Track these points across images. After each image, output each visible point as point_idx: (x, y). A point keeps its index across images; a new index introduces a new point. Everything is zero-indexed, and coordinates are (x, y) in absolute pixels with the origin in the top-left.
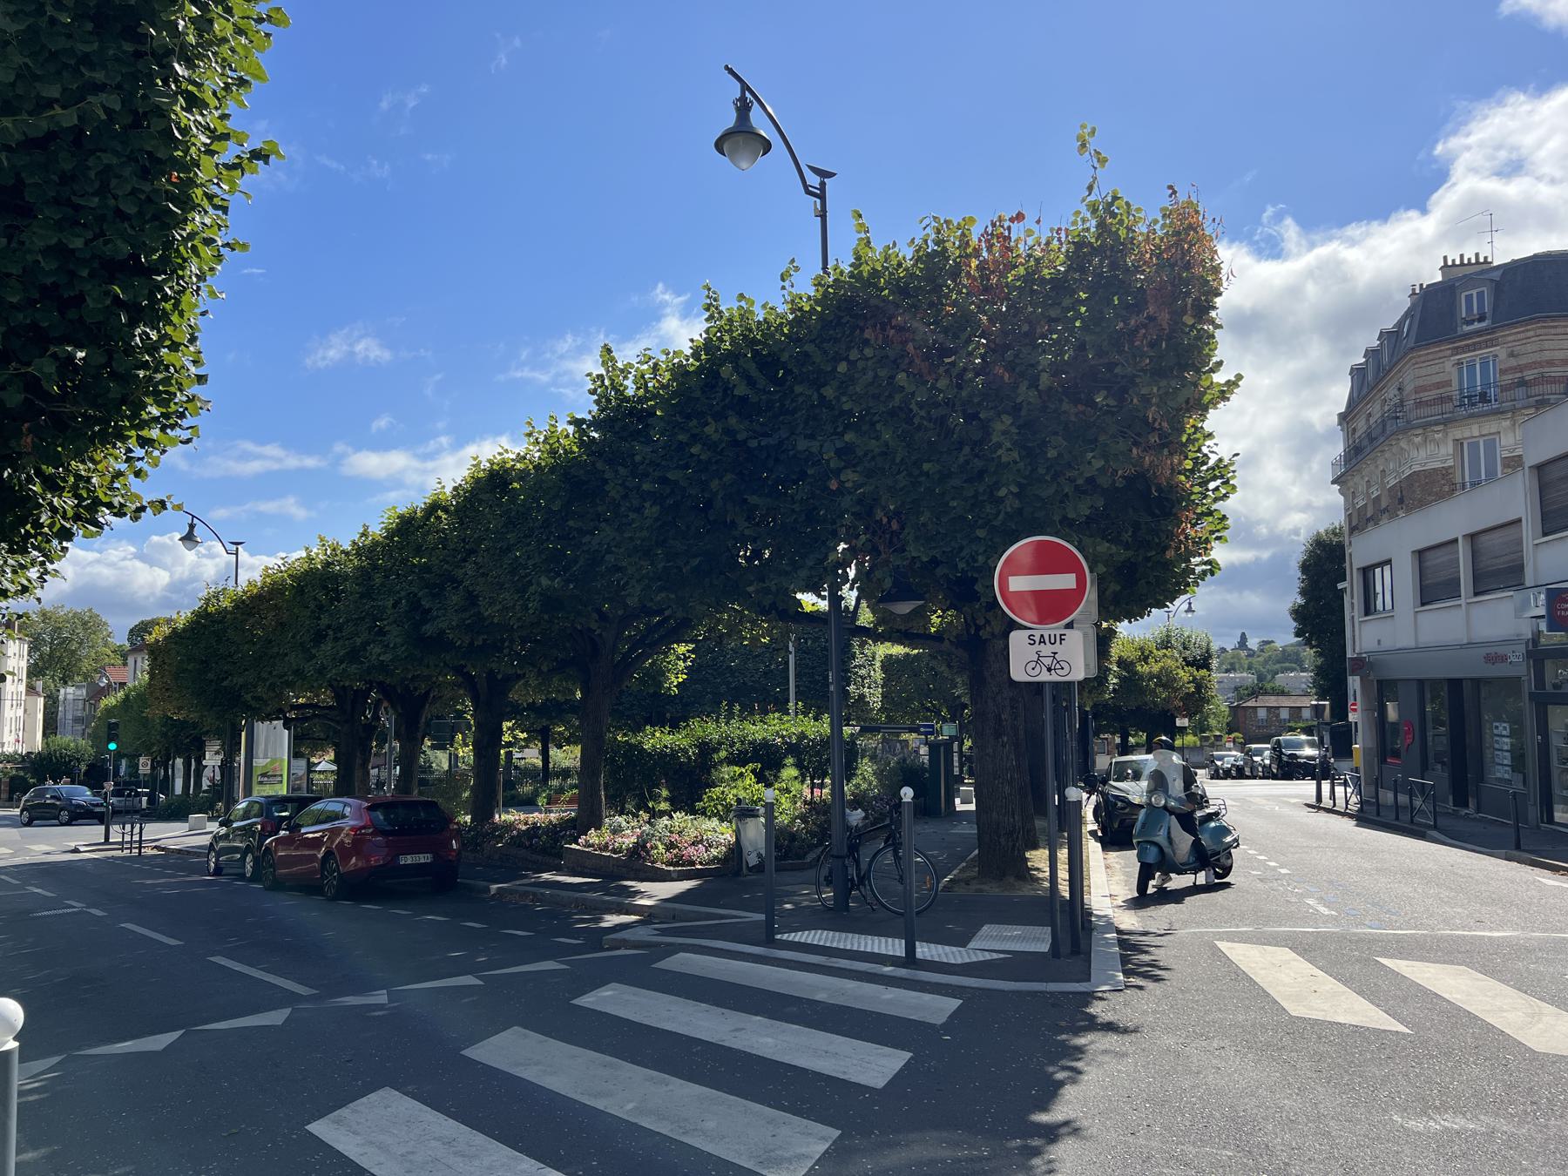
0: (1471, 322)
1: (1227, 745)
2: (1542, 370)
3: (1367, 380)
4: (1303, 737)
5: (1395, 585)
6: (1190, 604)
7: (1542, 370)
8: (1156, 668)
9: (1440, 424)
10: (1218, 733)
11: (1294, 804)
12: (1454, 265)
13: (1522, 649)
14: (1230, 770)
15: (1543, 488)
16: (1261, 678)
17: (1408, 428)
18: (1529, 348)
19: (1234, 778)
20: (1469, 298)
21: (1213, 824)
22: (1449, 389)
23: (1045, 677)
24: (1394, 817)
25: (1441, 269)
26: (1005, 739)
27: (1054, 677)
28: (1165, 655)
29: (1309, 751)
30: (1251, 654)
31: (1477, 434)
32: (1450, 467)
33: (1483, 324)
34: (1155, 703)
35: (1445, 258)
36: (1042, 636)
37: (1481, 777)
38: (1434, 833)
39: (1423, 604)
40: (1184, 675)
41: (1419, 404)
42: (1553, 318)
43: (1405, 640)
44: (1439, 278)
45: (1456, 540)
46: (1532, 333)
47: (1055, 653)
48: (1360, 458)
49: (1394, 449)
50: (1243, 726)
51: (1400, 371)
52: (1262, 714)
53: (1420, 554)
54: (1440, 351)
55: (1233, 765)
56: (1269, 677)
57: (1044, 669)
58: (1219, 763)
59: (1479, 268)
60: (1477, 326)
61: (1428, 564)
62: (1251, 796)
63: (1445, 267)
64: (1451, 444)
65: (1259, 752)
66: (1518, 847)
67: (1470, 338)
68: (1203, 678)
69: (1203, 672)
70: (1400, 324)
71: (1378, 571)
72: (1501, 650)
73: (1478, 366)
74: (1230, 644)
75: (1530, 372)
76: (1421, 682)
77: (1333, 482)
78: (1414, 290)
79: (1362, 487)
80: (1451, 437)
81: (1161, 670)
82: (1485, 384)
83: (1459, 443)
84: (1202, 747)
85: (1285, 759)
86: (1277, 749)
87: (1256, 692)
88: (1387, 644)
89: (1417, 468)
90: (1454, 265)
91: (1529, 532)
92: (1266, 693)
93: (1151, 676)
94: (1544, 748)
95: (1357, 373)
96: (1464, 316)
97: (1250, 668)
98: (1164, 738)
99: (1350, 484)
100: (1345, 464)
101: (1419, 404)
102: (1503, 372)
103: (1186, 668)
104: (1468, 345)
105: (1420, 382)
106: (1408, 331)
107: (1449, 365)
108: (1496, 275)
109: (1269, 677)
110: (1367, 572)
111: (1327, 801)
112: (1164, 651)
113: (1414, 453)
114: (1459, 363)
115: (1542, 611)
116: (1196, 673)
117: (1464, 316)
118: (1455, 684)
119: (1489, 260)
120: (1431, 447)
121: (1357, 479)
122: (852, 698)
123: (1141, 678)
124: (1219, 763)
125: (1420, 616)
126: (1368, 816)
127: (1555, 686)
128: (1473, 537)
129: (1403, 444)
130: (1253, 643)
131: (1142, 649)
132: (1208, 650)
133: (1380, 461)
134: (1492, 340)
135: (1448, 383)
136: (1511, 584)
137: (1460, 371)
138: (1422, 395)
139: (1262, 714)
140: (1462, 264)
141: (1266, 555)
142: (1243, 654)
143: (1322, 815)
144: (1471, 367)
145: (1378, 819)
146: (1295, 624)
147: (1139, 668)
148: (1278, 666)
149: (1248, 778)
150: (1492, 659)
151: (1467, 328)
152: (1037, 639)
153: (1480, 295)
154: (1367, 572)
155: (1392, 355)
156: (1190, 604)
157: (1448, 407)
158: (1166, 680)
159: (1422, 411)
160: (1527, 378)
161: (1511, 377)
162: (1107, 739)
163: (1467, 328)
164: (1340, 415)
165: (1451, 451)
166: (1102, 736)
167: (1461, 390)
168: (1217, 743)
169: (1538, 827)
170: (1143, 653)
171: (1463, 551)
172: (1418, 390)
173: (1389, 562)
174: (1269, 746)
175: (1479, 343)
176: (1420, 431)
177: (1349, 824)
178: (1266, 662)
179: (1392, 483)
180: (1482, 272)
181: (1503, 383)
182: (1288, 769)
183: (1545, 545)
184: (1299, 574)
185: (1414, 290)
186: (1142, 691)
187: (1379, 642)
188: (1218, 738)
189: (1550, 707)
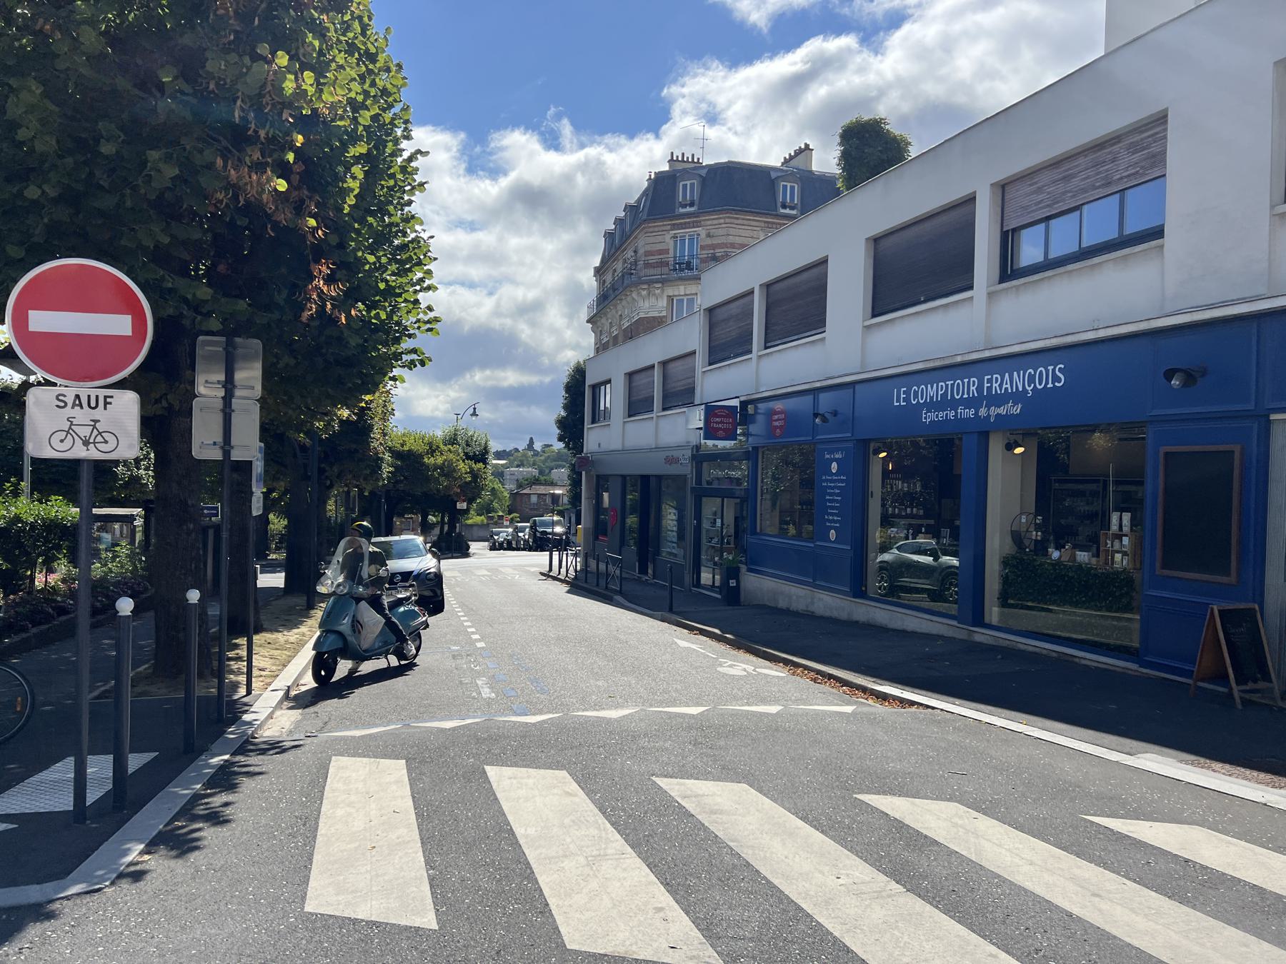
0: (685, 206)
1: (505, 523)
2: (726, 250)
3: (616, 242)
4: (556, 518)
5: (612, 399)
6: (475, 409)
7: (726, 250)
8: (440, 460)
9: (660, 282)
10: (501, 514)
11: (533, 572)
12: (677, 160)
13: (688, 453)
14: (503, 542)
15: (712, 326)
16: (541, 472)
17: (637, 284)
18: (721, 232)
19: (505, 549)
20: (685, 186)
21: (402, 609)
22: (667, 256)
23: (80, 452)
24: (595, 584)
25: (669, 162)
26: (191, 526)
27: (93, 454)
28: (450, 450)
29: (558, 529)
30: (536, 454)
31: (683, 293)
32: (664, 316)
33: (692, 209)
34: (438, 490)
35: (672, 153)
36: (78, 397)
37: (658, 552)
38: (618, 598)
39: (630, 416)
40: (463, 467)
41: (647, 265)
42: (737, 212)
43: (616, 444)
44: (666, 168)
45: (653, 367)
46: (722, 221)
47: (96, 421)
48: (606, 302)
49: (629, 299)
50: (519, 507)
51: (636, 238)
52: (534, 499)
53: (630, 375)
54: (663, 225)
55: (505, 539)
56: (547, 471)
57: (79, 442)
58: (496, 537)
59: (693, 165)
60: (688, 209)
61: (634, 384)
62: (503, 566)
63: (671, 161)
64: (665, 298)
65: (523, 529)
66: (671, 610)
67: (683, 219)
68: (479, 470)
69: (481, 465)
70: (639, 201)
71: (603, 388)
72: (676, 454)
73: (687, 241)
74: (522, 446)
75: (719, 250)
76: (624, 477)
77: (588, 322)
78: (650, 176)
79: (607, 327)
80: (665, 294)
81: (444, 464)
82: (691, 256)
83: (671, 299)
84: (488, 524)
85: (538, 535)
86: (533, 527)
87: (535, 482)
88: (605, 447)
89: (642, 315)
90: (677, 160)
91: (700, 361)
92: (541, 484)
93: (436, 467)
94: (698, 529)
95: (609, 236)
96: (680, 200)
97: (534, 464)
98: (365, 523)
99: (599, 324)
100: (597, 306)
101: (647, 265)
102: (703, 248)
103: (466, 461)
104: (681, 224)
105: (648, 248)
106: (644, 206)
107: (668, 237)
108: (703, 173)
109: (547, 471)
110: (595, 388)
111: (555, 572)
112: (450, 446)
113: (641, 303)
114: (675, 237)
115: (701, 425)
116: (474, 465)
117: (680, 200)
118: (645, 479)
119: (701, 161)
120: (653, 300)
121: (603, 320)
122: (121, 479)
123: (427, 466)
124: (496, 537)
125: (628, 425)
126: (579, 586)
127: (709, 483)
128: (664, 364)
129: (634, 295)
130: (538, 446)
131: (430, 444)
132: (486, 448)
133: (619, 307)
134: (696, 222)
135: (667, 251)
136: (686, 402)
137: (675, 242)
138: (649, 258)
139: (534, 499)
140: (683, 161)
141: (547, 379)
142: (530, 453)
143: (550, 582)
144: (683, 241)
145: (585, 585)
146: (558, 431)
147: (426, 460)
148: (554, 463)
149: (514, 549)
150: (671, 461)
151: (682, 210)
152: (70, 400)
153: (692, 185)
154: (595, 388)
155: (632, 224)
156: (475, 409)
157: (665, 270)
158: (448, 470)
159: (651, 271)
160: (717, 255)
161: (707, 252)
162: (412, 518)
163: (682, 210)
164: (595, 268)
165: (665, 305)
166: (406, 516)
167: (675, 257)
168: (499, 522)
169: (691, 590)
170: (431, 448)
171: (657, 375)
172: (648, 253)
173: (609, 381)
174: (528, 524)
175: (689, 223)
176: (645, 286)
177: (565, 588)
178: (546, 460)
179: (627, 325)
180: (695, 168)
181: (701, 256)
182: (540, 543)
183: (709, 373)
184: (564, 393)
185: (650, 176)
186: (428, 479)
187: (599, 444)
188: (501, 517)
189: (704, 499)
